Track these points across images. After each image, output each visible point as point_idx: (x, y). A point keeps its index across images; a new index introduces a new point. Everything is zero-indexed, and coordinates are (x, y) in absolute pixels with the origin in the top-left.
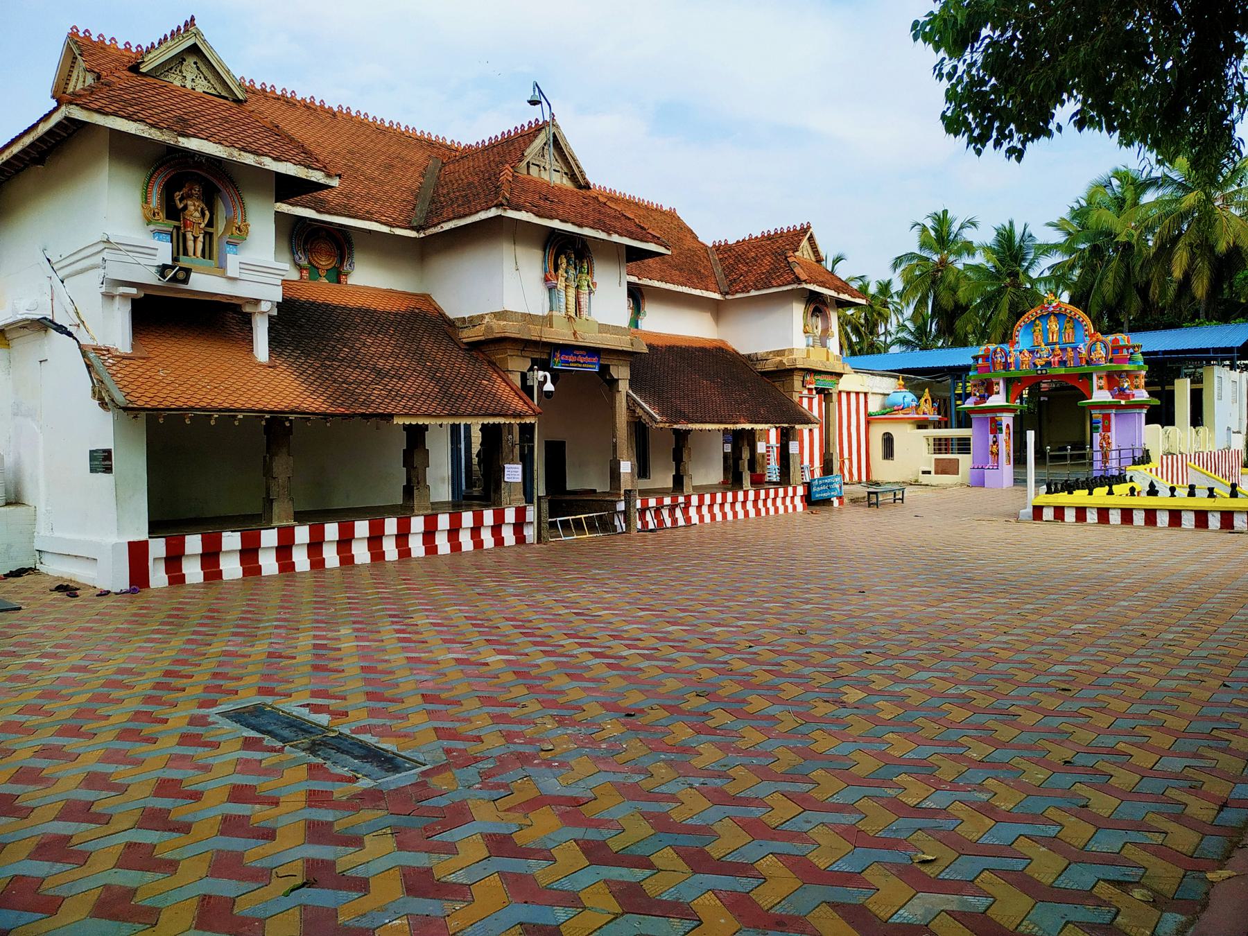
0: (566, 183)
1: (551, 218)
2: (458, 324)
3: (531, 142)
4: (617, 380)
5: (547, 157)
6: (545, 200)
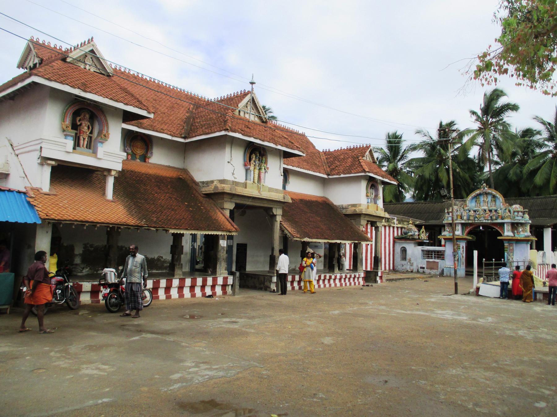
0: (257, 120)
1: (250, 136)
2: (200, 184)
3: (242, 100)
4: (276, 215)
5: (249, 107)
6: (247, 127)
